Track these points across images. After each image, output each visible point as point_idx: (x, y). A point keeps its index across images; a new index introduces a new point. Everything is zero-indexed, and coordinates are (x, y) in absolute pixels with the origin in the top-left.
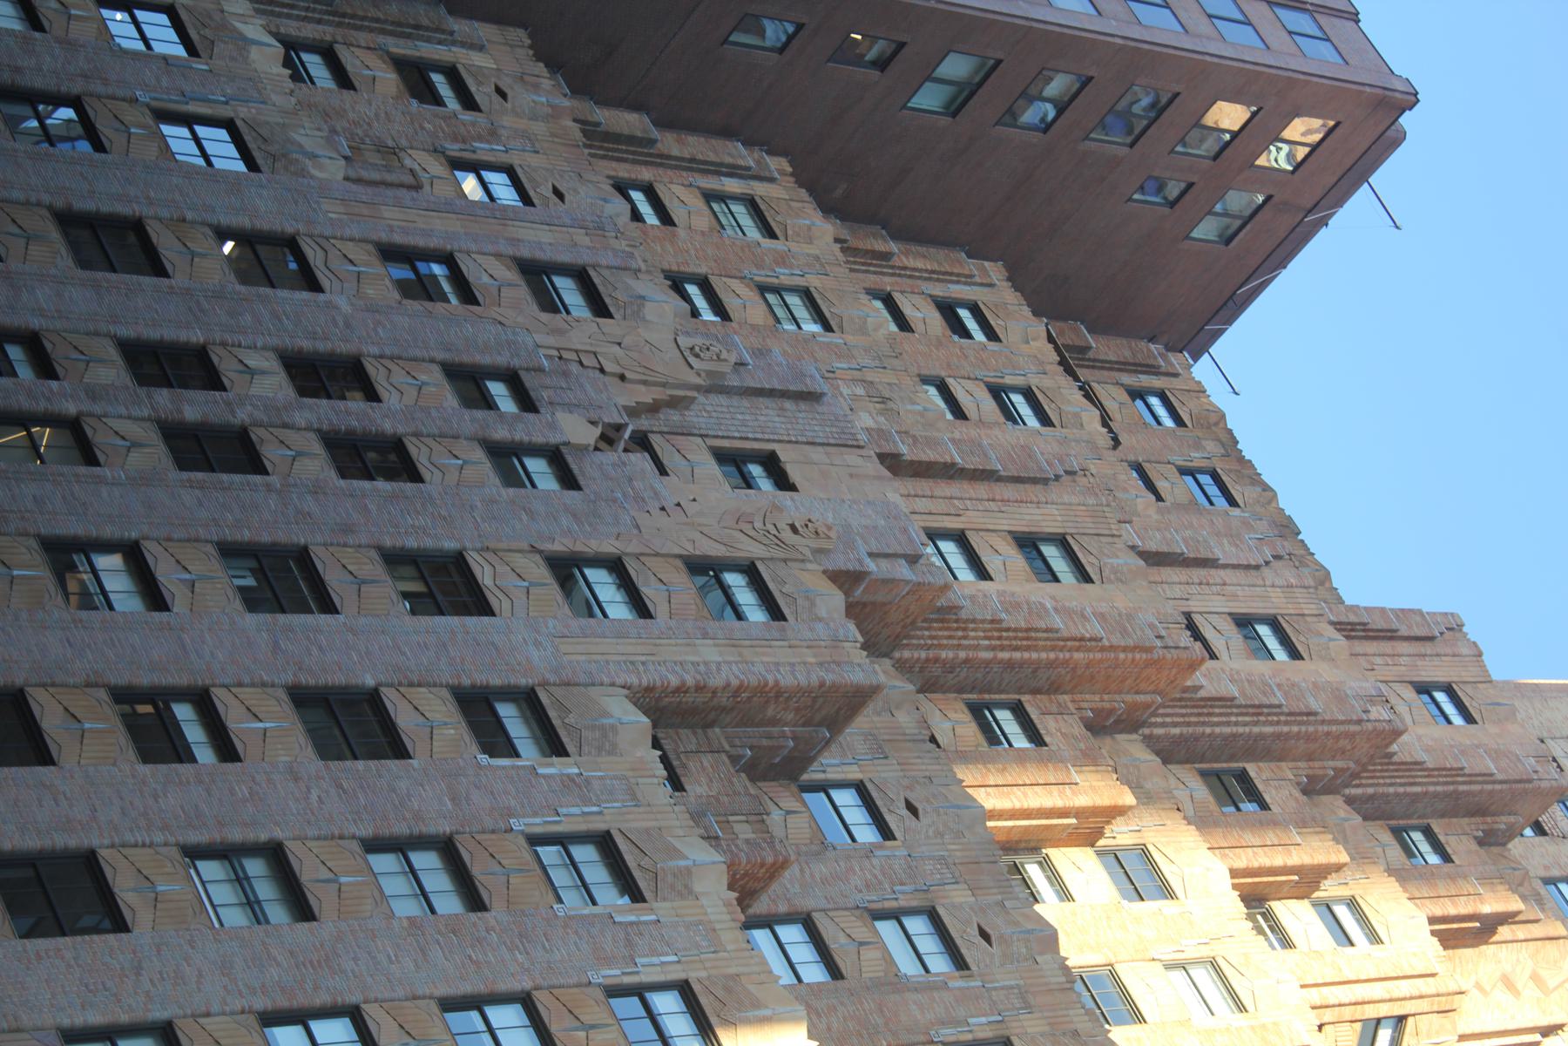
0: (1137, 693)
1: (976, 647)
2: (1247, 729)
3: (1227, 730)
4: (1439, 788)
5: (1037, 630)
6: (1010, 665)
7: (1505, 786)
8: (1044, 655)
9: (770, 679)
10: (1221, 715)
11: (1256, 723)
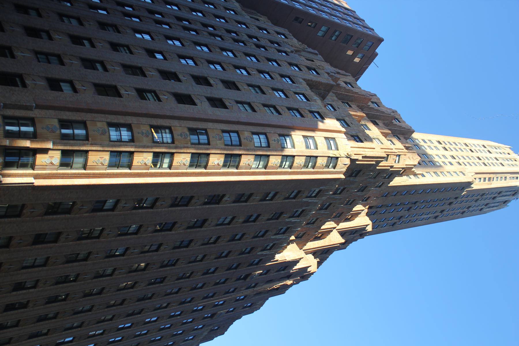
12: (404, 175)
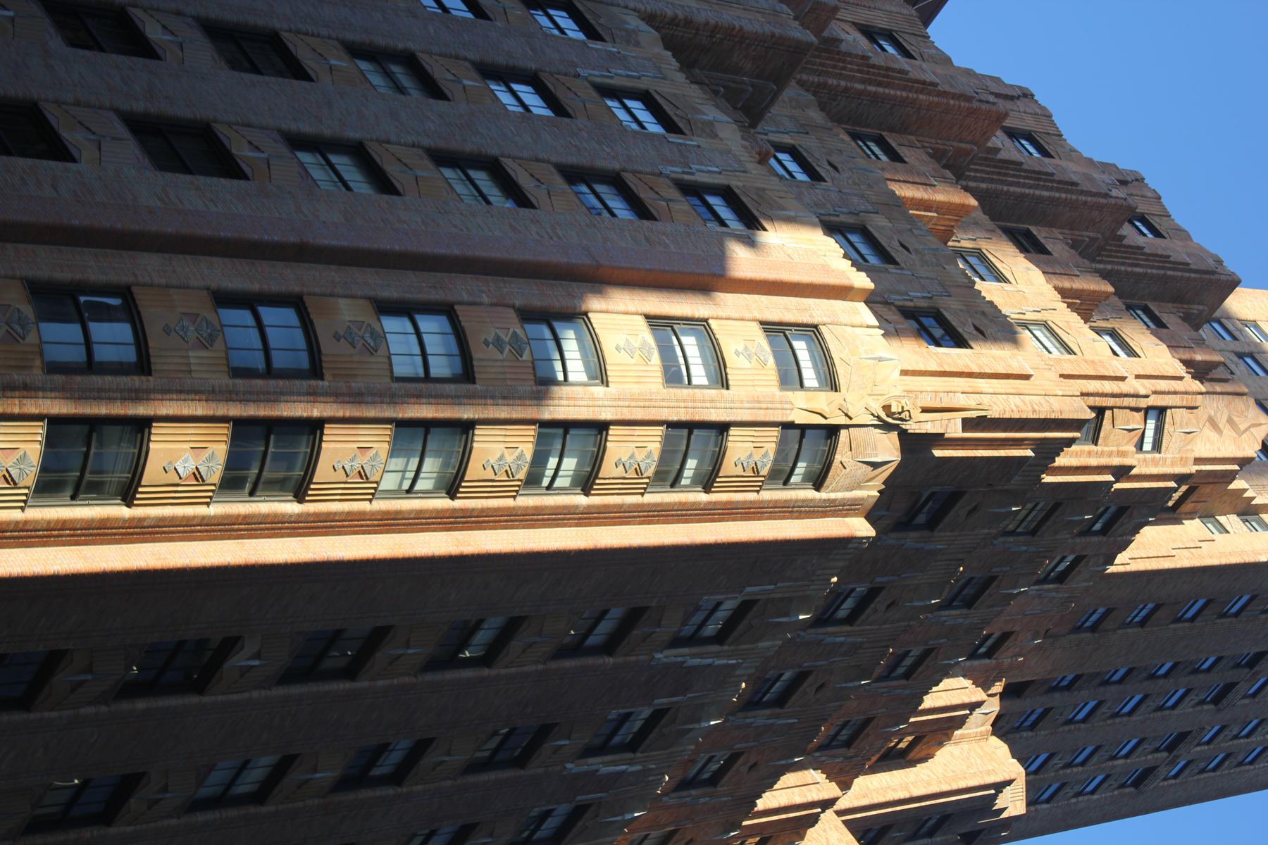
0: (960, 141)
1: (852, 79)
2: (1031, 191)
3: (1018, 190)
4: (1154, 271)
5: (893, 70)
6: (875, 97)
7: (1198, 276)
8: (899, 93)
9: (737, 24)
10: (1013, 176)
11: (1037, 187)
12: (1191, 516)
